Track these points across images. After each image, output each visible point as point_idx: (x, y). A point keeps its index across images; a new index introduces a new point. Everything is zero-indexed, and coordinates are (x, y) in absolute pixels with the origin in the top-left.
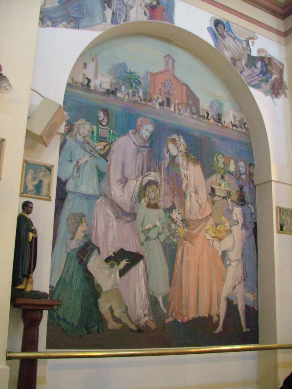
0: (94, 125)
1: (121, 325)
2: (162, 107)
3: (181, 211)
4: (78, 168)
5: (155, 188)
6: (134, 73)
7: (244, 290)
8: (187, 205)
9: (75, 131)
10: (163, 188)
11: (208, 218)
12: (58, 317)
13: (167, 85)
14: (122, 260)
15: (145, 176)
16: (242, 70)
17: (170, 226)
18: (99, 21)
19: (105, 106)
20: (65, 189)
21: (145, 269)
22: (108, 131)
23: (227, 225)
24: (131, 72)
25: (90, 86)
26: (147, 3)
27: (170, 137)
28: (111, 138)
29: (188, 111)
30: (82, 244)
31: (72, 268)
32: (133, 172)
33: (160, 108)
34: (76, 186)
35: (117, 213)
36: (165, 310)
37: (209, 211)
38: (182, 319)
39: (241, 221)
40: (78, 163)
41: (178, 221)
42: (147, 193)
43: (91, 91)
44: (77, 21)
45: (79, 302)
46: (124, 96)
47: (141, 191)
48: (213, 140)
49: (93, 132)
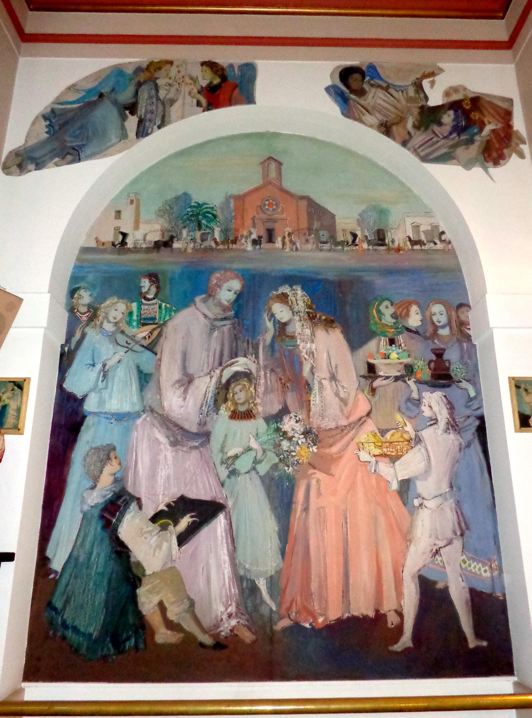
0: (133, 302)
1: (181, 635)
2: (258, 247)
3: (300, 417)
4: (105, 374)
5: (246, 384)
6: (205, 204)
7: (464, 557)
8: (313, 404)
9: (101, 318)
10: (262, 381)
11: (361, 422)
12: (65, 625)
13: (267, 207)
14: (183, 515)
15: (227, 366)
16: (407, 137)
17: (278, 446)
18: (114, 140)
19: (152, 268)
20: (82, 411)
21: (228, 528)
22: (157, 306)
23: (409, 428)
24: (199, 204)
25: (126, 244)
26: (202, 87)
27: (275, 293)
28: (163, 316)
29: (311, 241)
30: (110, 496)
31: (90, 538)
32: (204, 364)
33: (255, 248)
34: (101, 402)
35: (173, 436)
36: (273, 604)
37: (363, 407)
38: (311, 621)
39: (443, 416)
40: (104, 365)
41: (296, 435)
42: (231, 394)
43: (129, 250)
44: (77, 150)
45: (101, 596)
46: (186, 244)
47: (218, 393)
48: (367, 278)
49: (131, 314)
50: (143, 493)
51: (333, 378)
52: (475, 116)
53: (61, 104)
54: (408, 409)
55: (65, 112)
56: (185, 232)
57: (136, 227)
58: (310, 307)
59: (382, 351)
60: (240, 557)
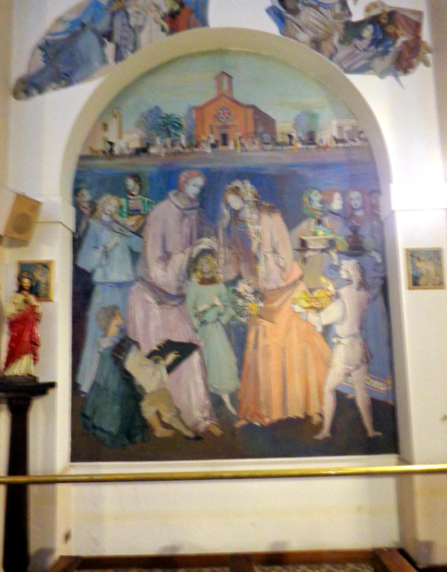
2: (216, 149)
12: (94, 427)
19: (134, 170)
34: (105, 275)
35: (160, 298)
43: (117, 157)
50: (140, 338)
51: (275, 251)
52: (390, 29)
53: (52, 34)
54: (331, 273)
55: (56, 42)
56: (158, 141)
57: (120, 136)
58: (256, 197)
59: (313, 230)
60: (210, 381)
